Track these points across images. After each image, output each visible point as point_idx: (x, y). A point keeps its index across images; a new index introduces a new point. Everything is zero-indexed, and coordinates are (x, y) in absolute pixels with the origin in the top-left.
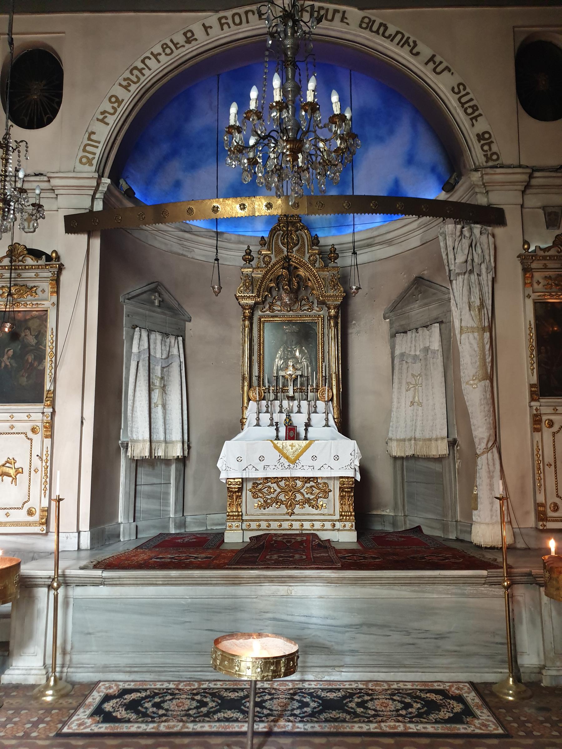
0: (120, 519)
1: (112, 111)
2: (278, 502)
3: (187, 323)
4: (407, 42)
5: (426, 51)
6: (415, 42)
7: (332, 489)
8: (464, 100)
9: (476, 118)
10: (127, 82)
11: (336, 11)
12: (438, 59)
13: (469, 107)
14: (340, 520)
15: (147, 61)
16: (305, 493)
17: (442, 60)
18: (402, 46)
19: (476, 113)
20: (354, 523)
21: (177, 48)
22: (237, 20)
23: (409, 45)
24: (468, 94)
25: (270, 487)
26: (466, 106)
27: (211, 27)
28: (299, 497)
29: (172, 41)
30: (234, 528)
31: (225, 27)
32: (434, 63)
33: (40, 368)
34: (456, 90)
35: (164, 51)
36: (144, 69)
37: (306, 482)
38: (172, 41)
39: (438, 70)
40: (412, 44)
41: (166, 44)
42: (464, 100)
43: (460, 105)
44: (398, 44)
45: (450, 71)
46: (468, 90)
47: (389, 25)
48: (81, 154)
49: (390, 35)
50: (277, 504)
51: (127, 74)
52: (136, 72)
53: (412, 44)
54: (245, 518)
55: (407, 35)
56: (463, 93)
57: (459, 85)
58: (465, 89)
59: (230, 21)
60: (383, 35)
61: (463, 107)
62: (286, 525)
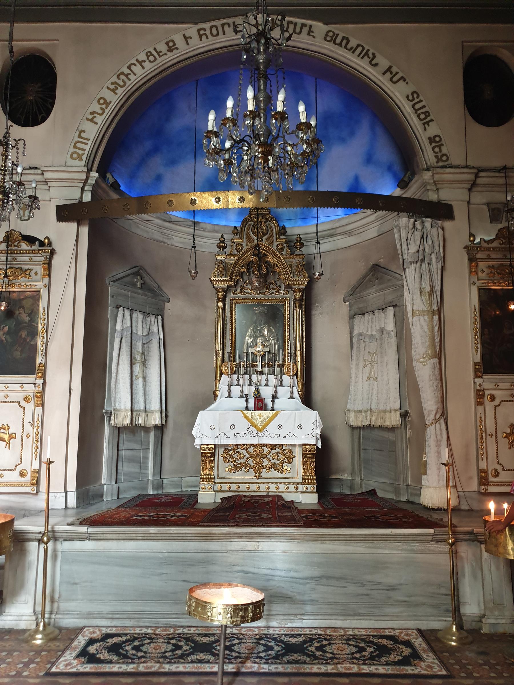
0: (104, 481)
1: (100, 112)
2: (246, 467)
3: (166, 304)
4: (367, 54)
5: (384, 62)
6: (374, 54)
7: (296, 455)
8: (417, 106)
9: (428, 123)
10: (114, 86)
11: (303, 25)
12: (394, 70)
13: (422, 113)
14: (302, 484)
15: (133, 67)
16: (271, 459)
17: (397, 70)
18: (362, 58)
19: (428, 119)
20: (315, 486)
21: (424, 124)
22: (214, 32)
23: (369, 57)
24: (421, 101)
25: (239, 453)
26: (419, 112)
27: (191, 38)
28: (266, 462)
29: (155, 49)
30: (207, 490)
31: (204, 37)
32: (391, 73)
33: (33, 343)
34: (411, 98)
35: (148, 59)
36: (130, 74)
37: (272, 449)
38: (155, 49)
39: (395, 79)
40: (371, 56)
41: (150, 52)
42: (417, 106)
43: (414, 111)
44: (359, 56)
45: (405, 80)
46: (421, 98)
47: (351, 38)
48: (72, 150)
49: (352, 48)
50: (246, 468)
51: (114, 79)
52: (122, 77)
53: (371, 56)
54: (217, 480)
55: (367, 48)
56: (416, 100)
57: (413, 93)
58: (418, 97)
59: (208, 32)
60: (346, 47)
61: (416, 113)
62: (254, 487)
